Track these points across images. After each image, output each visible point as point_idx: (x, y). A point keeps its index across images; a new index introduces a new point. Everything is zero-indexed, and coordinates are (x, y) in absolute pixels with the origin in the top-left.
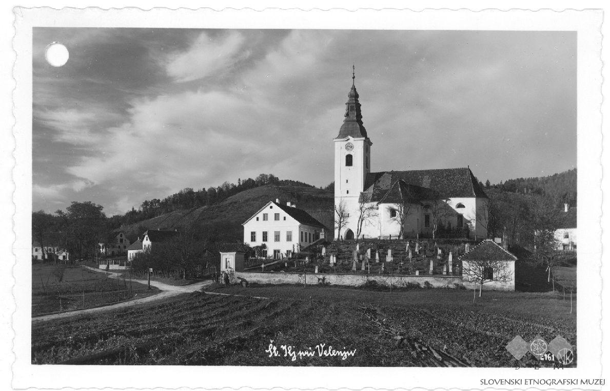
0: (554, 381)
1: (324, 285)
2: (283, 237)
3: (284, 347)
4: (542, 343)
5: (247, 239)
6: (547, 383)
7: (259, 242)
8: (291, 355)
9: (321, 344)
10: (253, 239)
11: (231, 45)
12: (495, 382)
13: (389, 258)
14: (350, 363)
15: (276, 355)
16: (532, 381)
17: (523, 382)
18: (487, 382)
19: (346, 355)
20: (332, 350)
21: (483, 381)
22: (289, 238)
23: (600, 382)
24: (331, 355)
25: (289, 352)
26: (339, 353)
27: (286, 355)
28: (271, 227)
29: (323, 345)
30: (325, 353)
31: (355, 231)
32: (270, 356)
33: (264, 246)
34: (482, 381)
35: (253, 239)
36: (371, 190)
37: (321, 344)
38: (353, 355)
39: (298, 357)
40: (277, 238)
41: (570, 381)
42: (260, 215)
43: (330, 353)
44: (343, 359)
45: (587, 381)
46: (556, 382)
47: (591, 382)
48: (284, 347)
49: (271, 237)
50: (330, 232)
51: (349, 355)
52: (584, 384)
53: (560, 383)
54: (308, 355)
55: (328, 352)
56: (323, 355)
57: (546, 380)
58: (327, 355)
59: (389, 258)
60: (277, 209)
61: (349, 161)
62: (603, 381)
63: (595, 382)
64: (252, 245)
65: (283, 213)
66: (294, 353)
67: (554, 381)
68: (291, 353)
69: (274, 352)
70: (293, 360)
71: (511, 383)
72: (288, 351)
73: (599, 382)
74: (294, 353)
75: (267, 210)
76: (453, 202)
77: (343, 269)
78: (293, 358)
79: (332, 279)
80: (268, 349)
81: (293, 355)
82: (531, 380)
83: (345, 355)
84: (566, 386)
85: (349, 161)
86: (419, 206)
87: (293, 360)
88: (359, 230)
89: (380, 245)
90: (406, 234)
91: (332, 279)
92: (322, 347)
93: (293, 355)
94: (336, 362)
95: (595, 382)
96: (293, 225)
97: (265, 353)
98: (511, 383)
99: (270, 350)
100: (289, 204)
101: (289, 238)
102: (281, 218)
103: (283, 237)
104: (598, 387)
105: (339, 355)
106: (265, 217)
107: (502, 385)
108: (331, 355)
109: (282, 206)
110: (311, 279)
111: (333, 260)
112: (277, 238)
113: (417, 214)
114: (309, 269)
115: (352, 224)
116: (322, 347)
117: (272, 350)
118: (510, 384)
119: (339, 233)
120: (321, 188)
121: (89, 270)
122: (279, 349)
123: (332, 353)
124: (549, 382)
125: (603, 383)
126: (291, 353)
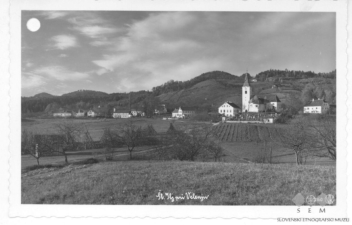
0: (320, 219)
1: (241, 123)
2: (229, 111)
3: (167, 194)
4: (313, 197)
5: (220, 112)
6: (315, 220)
7: (223, 113)
8: (171, 199)
9: (188, 192)
10: (221, 112)
11: (334, 143)
12: (285, 220)
13: (254, 117)
14: (206, 203)
15: (162, 199)
16: (307, 220)
17: (302, 220)
18: (281, 220)
19: (203, 199)
20: (195, 195)
21: (279, 219)
22: (231, 112)
23: (346, 219)
24: (194, 198)
25: (170, 197)
26: (199, 197)
27: (168, 199)
28: (226, 108)
29: (189, 193)
30: (191, 198)
31: (247, 110)
32: (159, 199)
33: (224, 114)
34: (278, 219)
35: (221, 112)
36: (252, 99)
37: (188, 192)
38: (207, 198)
39: (175, 199)
40: (228, 112)
41: (329, 219)
42: (223, 106)
43: (193, 197)
44: (201, 201)
45: (339, 219)
46: (321, 220)
47: (341, 220)
48: (167, 194)
49: (226, 111)
50: (242, 110)
51: (205, 198)
52: (337, 221)
53: (323, 220)
54: (181, 199)
55: (192, 197)
56: (190, 199)
57: (315, 219)
58: (192, 199)
59: (254, 117)
60: (227, 104)
61: (246, 92)
62: (348, 219)
63: (343, 220)
64: (221, 113)
65: (229, 105)
66: (173, 197)
67: (320, 219)
68: (171, 197)
69: (161, 197)
70: (172, 201)
71: (295, 220)
72: (169, 196)
73: (345, 220)
74: (173, 197)
75: (225, 104)
76: (272, 103)
77: (244, 120)
78: (172, 200)
79: (242, 122)
80: (158, 195)
81: (172, 199)
82: (306, 219)
83: (202, 198)
84: (327, 222)
85: (246, 92)
86: (263, 104)
87: (172, 201)
88: (248, 109)
89: (252, 114)
90: (260, 112)
91: (242, 122)
92: (189, 194)
93: (172, 199)
94: (197, 202)
95: (343, 220)
96: (232, 108)
97: (156, 197)
98: (295, 220)
99: (159, 195)
100: (230, 102)
101: (231, 112)
102: (229, 106)
103: (229, 111)
104: (346, 223)
105: (199, 198)
106: (224, 106)
107: (290, 222)
108: (194, 198)
109: (228, 103)
110: (239, 122)
111: (242, 118)
112: (228, 112)
113: (262, 106)
114: (237, 120)
115: (247, 108)
116: (189, 194)
117: (160, 196)
118: (294, 221)
119: (244, 111)
120: (148, 91)
121: (63, 144)
122: (164, 195)
123: (195, 197)
124: (317, 220)
125: (348, 220)
126: (171, 197)
